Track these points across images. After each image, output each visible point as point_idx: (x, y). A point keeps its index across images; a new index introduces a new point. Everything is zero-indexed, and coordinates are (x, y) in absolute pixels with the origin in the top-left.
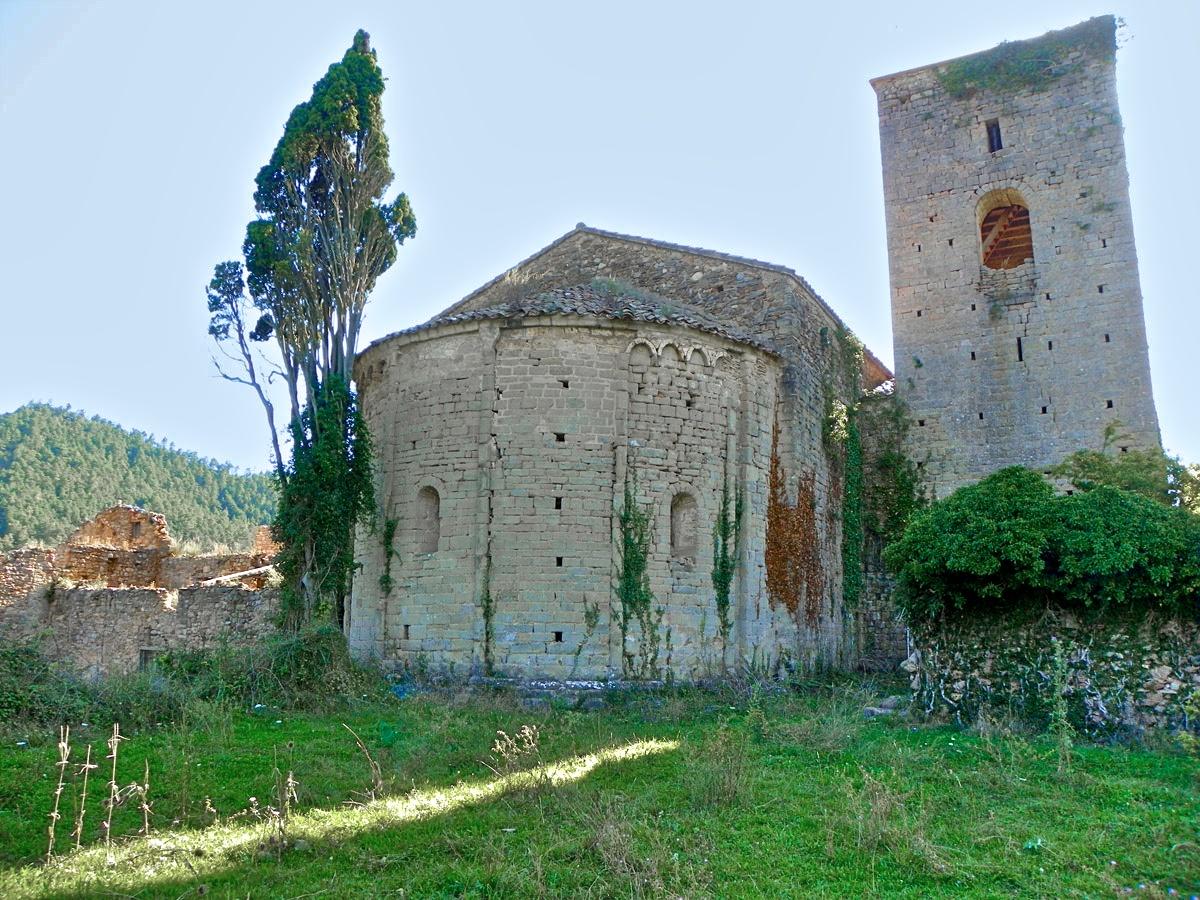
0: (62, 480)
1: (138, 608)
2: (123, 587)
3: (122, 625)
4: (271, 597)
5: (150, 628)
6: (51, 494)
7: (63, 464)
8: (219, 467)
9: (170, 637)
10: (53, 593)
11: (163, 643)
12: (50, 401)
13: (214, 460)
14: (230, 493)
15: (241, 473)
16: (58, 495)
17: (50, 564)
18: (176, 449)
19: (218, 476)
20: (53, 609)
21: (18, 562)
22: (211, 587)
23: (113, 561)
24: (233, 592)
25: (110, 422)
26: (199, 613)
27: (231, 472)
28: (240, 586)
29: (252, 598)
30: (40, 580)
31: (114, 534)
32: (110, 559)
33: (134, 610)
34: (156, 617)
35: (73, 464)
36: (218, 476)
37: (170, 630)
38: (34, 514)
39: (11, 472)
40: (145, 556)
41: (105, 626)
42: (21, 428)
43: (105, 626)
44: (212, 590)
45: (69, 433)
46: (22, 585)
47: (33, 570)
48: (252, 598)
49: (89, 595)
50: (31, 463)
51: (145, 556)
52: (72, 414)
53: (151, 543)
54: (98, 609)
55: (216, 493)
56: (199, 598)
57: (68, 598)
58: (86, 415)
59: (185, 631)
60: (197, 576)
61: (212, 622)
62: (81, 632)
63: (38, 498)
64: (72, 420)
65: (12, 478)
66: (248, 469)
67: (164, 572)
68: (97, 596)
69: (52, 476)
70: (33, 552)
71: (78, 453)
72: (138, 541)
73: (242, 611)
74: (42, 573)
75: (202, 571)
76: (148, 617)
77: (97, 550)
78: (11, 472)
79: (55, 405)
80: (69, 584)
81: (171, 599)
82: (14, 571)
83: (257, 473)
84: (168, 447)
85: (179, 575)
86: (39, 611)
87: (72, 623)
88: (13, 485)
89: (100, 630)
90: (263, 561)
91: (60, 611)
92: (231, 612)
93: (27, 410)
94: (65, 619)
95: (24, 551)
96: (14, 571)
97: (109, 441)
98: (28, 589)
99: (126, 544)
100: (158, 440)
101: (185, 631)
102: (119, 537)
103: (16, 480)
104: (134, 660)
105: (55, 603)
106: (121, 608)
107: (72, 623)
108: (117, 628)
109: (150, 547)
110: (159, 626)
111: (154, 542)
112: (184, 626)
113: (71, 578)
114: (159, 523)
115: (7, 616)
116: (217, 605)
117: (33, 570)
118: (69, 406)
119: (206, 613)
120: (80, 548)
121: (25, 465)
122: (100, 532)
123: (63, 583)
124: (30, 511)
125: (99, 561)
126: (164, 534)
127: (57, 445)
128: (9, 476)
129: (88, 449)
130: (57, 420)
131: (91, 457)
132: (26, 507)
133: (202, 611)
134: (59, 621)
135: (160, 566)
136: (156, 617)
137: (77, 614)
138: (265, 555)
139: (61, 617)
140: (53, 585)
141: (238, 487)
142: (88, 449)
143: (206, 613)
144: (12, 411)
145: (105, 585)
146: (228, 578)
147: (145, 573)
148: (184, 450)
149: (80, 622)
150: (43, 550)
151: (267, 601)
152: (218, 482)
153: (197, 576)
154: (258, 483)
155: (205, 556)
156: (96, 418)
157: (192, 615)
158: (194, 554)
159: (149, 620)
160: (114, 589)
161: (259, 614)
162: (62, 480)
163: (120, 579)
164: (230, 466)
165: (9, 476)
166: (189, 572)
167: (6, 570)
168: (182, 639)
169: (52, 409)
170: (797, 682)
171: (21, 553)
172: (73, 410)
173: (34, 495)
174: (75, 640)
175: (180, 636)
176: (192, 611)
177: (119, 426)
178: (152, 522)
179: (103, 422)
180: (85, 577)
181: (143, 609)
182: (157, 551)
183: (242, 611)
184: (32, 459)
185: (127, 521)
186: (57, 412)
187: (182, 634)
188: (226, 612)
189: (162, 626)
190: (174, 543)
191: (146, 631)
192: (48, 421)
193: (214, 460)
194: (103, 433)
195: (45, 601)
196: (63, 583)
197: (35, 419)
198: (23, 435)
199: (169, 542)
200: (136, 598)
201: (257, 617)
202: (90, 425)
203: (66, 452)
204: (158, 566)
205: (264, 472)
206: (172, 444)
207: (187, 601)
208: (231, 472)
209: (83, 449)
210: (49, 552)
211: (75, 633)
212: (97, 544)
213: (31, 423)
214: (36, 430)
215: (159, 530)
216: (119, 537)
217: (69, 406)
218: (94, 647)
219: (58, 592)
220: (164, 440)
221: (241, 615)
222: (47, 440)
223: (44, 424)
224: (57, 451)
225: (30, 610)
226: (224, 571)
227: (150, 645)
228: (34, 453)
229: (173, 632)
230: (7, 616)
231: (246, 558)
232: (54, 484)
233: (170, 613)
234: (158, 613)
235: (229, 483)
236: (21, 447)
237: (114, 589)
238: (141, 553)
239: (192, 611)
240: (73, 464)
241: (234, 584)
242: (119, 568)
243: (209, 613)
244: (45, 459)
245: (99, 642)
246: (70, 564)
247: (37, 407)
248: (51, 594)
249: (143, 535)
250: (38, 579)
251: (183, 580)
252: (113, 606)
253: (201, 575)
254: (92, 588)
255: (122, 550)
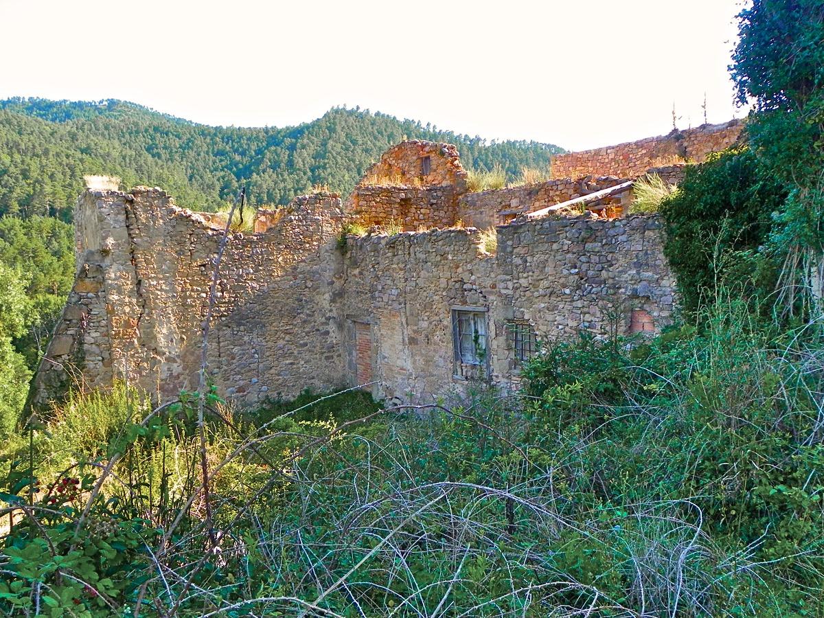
0: (361, 163)
1: (443, 256)
2: (422, 230)
3: (427, 279)
4: (644, 228)
5: (462, 281)
6: (354, 174)
7: (360, 151)
8: (471, 141)
9: (491, 293)
10: (345, 243)
11: (481, 301)
12: (345, 105)
13: (466, 136)
14: (482, 160)
15: (488, 144)
16: (359, 174)
17: (337, 210)
18: (437, 131)
19: (471, 148)
20: (347, 262)
21: (303, 211)
22: (543, 220)
23: (405, 202)
24: (580, 225)
25: (388, 116)
26: (529, 259)
27: (480, 144)
28: (588, 215)
29: (611, 232)
30: (330, 230)
31: (403, 174)
32: (402, 200)
33: (439, 258)
34: (469, 266)
35: (367, 151)
36: (471, 148)
37: (488, 283)
38: (345, 190)
39: (326, 161)
40: (439, 194)
41: (406, 280)
42: (328, 128)
43: (406, 280)
44: (546, 225)
45: (361, 127)
46: (311, 237)
47: (320, 218)
48: (611, 232)
49: (383, 242)
50: (339, 153)
51: (439, 194)
52: (361, 114)
53: (444, 178)
54: (395, 259)
55: (471, 161)
56: (526, 236)
57: (361, 247)
58: (370, 113)
59: (510, 285)
60: (503, 212)
61: (549, 270)
62: (380, 288)
63: (347, 178)
64: (362, 118)
65: (327, 166)
66: (493, 141)
67: (462, 210)
68: (392, 244)
69: (354, 161)
70: (318, 198)
71: (369, 142)
72: (430, 178)
73: (596, 253)
74: (330, 221)
75: (510, 206)
76: (458, 267)
77: (387, 190)
78: (326, 161)
79: (349, 108)
80: (362, 232)
81: (487, 241)
82: (299, 220)
83: (500, 142)
84: (431, 130)
85: (481, 213)
86: (333, 266)
87: (369, 277)
88: (329, 170)
89: (401, 285)
90: (588, 185)
91: (355, 264)
92: (579, 254)
93: (331, 115)
94: (361, 273)
95: (307, 196)
96: (299, 220)
97: (389, 130)
98: (318, 240)
99: (417, 183)
100: (424, 125)
101: (510, 285)
102: (408, 176)
103: (330, 167)
104: (445, 323)
105: (348, 255)
106: (423, 256)
107: (369, 277)
108: (421, 282)
109: (444, 184)
110: (473, 278)
111: (447, 177)
112: (509, 277)
113: (362, 224)
114: (450, 155)
115: (300, 273)
116: (555, 246)
117: (320, 218)
118: (358, 108)
119: (539, 257)
120: (367, 189)
121: (335, 155)
122: (389, 173)
123: (354, 231)
124: (342, 188)
125: (390, 203)
126: (458, 167)
127: (354, 138)
128: (325, 164)
129: (376, 138)
130: (351, 119)
131: (378, 144)
132: (339, 185)
133: (532, 256)
134: (355, 275)
135: (458, 205)
136: (469, 266)
137: (373, 267)
138: (589, 178)
139: (356, 271)
140: (344, 235)
141: (487, 156)
142: (376, 138)
143: (539, 257)
144: (321, 117)
145: (399, 230)
146: (565, 205)
147: (442, 214)
148: (444, 131)
149: (377, 276)
150: (328, 193)
151: (637, 236)
152: (472, 153)
153: (503, 212)
154: (502, 150)
155: (511, 186)
156: (378, 114)
157: (518, 261)
158: (497, 187)
159: (460, 270)
160: (412, 233)
161: (625, 255)
162: (361, 163)
163: (416, 223)
164: (479, 140)
165: (325, 164)
166: (492, 208)
167: (291, 221)
168: (507, 296)
169: (347, 112)
170: (573, 279)
171: (305, 199)
172: (361, 110)
173: (343, 177)
174: (373, 298)
175: (503, 291)
176: (518, 255)
177: (394, 118)
178: (442, 154)
179: (383, 116)
180: (378, 223)
181: (450, 257)
182: (452, 188)
183: (596, 253)
184: (339, 150)
185: (415, 158)
186: (351, 113)
187: (507, 288)
188: (570, 255)
189: (479, 278)
190: (471, 176)
191: (457, 285)
192: (346, 121)
193: (466, 136)
194: (384, 125)
195: (338, 253)
196: (354, 231)
197: (337, 121)
198: (330, 133)
199: (465, 175)
200: (440, 243)
201: (622, 261)
202: (374, 120)
203: (360, 142)
204: (456, 204)
205: (506, 142)
206: (434, 127)
207: (510, 243)
208: (480, 144)
209: (372, 138)
210: (335, 196)
211: (372, 290)
212: (385, 183)
213: (335, 124)
214: (338, 128)
215: (452, 163)
216: (408, 176)
217: (358, 108)
218: (395, 305)
219: (350, 242)
220: (428, 125)
221: (595, 259)
222: (347, 135)
223: (343, 123)
224: (354, 142)
225: (323, 265)
226: (537, 204)
227: (464, 303)
228: (339, 145)
229: (494, 286)
230: (300, 273)
231: (567, 183)
232: (356, 166)
233: (488, 260)
234: (471, 261)
235: (480, 153)
236: (331, 142)
237: (412, 233)
238: (436, 190)
239: (518, 255)
240: (367, 151)
241: (576, 213)
242: (413, 210)
243: (543, 258)
244: (347, 149)
245: (402, 300)
246: (359, 208)
247: (337, 111)
248: (343, 245)
249: (435, 171)
250: (327, 228)
251: (487, 219)
252: (413, 255)
253: (508, 211)
254: (386, 234)
255: (415, 189)
